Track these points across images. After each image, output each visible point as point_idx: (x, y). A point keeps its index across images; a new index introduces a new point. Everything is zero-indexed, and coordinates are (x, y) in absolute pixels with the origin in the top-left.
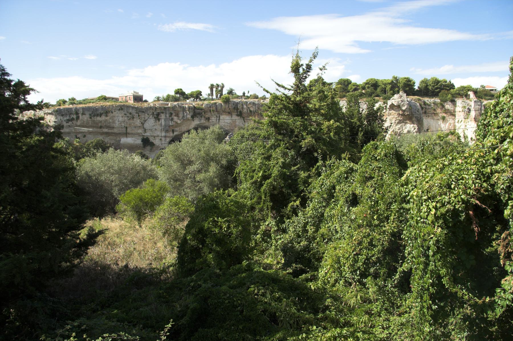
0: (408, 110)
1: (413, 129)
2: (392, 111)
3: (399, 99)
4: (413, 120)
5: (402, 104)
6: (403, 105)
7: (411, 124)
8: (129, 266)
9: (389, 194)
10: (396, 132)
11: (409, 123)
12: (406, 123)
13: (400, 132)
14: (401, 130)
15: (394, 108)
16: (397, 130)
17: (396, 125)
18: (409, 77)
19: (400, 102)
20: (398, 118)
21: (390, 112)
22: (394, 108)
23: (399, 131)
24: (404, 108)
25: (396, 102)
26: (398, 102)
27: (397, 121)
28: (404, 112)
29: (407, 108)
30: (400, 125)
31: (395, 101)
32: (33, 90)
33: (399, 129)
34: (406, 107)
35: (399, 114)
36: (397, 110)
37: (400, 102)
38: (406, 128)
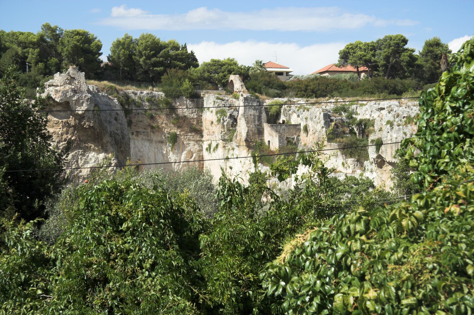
3: (68, 87)
4: (105, 141)
5: (75, 98)
7: (99, 152)
11: (94, 150)
12: (87, 150)
19: (70, 94)
20: (64, 136)
24: (80, 110)
25: (60, 94)
28: (80, 121)
31: (57, 92)
34: (84, 107)
35: (67, 125)
36: (62, 114)
37: (70, 94)
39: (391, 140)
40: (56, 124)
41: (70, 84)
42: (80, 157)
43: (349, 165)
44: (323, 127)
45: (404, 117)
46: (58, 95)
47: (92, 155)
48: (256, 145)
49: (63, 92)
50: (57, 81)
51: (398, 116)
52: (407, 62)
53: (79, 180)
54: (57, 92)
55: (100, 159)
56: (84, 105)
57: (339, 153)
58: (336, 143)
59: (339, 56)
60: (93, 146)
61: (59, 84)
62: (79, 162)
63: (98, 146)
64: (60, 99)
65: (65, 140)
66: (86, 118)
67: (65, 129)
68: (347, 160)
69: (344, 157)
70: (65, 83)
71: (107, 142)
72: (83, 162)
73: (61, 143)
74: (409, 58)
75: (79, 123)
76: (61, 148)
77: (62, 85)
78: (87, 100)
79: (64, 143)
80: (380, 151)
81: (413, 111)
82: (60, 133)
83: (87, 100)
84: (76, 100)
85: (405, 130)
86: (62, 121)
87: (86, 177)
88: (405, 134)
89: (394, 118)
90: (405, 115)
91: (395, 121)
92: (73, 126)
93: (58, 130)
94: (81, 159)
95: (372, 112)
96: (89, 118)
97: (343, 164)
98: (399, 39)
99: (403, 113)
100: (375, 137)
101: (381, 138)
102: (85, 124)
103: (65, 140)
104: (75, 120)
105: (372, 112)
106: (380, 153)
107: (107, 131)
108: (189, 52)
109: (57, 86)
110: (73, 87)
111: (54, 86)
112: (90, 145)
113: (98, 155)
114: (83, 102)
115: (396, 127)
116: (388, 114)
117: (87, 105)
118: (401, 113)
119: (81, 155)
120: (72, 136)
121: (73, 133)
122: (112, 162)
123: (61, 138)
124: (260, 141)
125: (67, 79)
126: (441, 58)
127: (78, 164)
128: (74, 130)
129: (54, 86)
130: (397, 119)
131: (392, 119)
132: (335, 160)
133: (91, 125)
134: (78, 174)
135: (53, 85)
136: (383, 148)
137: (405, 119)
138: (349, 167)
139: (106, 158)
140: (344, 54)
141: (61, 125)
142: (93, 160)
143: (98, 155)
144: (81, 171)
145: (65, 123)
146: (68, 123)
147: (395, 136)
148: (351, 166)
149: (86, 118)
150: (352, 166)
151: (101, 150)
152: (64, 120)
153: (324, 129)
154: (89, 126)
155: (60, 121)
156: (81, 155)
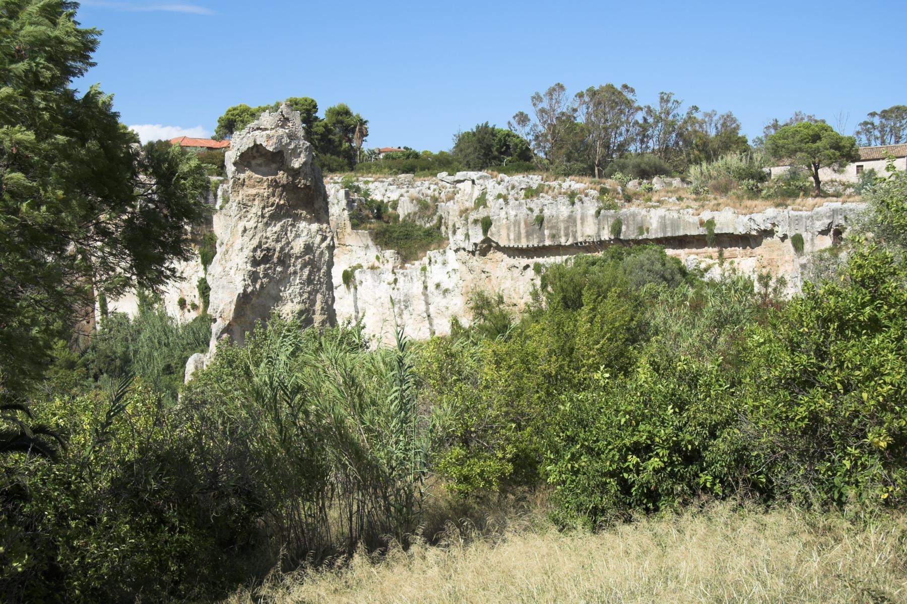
0: (308, 170)
1: (319, 238)
2: (248, 173)
3: (281, 131)
4: (316, 206)
5: (292, 146)
6: (295, 153)
7: (310, 222)
8: (416, 494)
9: (549, 412)
10: (268, 249)
11: (305, 219)
12: (297, 218)
13: (282, 249)
14: (284, 242)
15: (253, 162)
16: (270, 244)
17: (267, 225)
18: (549, 87)
19: (285, 140)
20: (272, 200)
21: (242, 176)
22: (253, 162)
23: (278, 246)
24: (296, 164)
25: (275, 140)
26: (280, 138)
27: (268, 211)
28: (294, 179)
29: (305, 164)
30: (279, 225)
31: (269, 137)
32: (255, 141)
33: (278, 241)
34: (302, 159)
35: (275, 184)
36: (263, 169)
37: (285, 140)
38: (297, 236)
39: (507, 218)
40: (259, 182)
41: (282, 127)
42: (289, 229)
43: (388, 258)
44: (344, 209)
45: (522, 189)
46: (271, 142)
47: (303, 225)
48: (204, 238)
49: (277, 138)
50: (265, 123)
51: (513, 188)
52: (321, 134)
53: (290, 260)
54: (269, 137)
55: (312, 231)
56: (302, 155)
57: (370, 243)
58: (366, 230)
59: (217, 124)
60: (304, 212)
61: (269, 127)
62: (289, 235)
63: (311, 215)
64: (274, 147)
65: (272, 205)
66: (303, 174)
67: (271, 190)
68: (383, 252)
69: (380, 249)
70: (277, 126)
71: (320, 208)
72: (293, 235)
73: (267, 210)
74: (324, 130)
75: (292, 181)
76: (267, 215)
77: (273, 129)
78: (306, 150)
79: (270, 208)
80: (489, 233)
81: (534, 181)
82: (266, 194)
83: (306, 150)
84: (293, 149)
85: (533, 206)
86: (268, 179)
87: (299, 255)
88: (531, 210)
89: (508, 190)
90: (523, 186)
91: (509, 194)
92: (283, 186)
93: (262, 190)
94: (291, 231)
95: (386, 191)
96: (306, 174)
97: (378, 258)
98: (310, 104)
99: (520, 183)
100: (478, 216)
101: (488, 217)
102: (300, 182)
103: (272, 205)
104: (287, 177)
105: (386, 191)
106: (489, 236)
107: (321, 193)
108: (113, 110)
109: (266, 129)
110: (287, 131)
111: (261, 129)
112: (300, 211)
113: (309, 225)
114: (301, 152)
115: (512, 202)
116: (497, 185)
117: (306, 156)
118: (517, 184)
119: (291, 225)
120: (280, 200)
121: (281, 195)
122: (328, 235)
123: (267, 203)
124: (208, 234)
125: (280, 120)
126: (353, 132)
127: (287, 238)
128: (283, 192)
129: (261, 129)
130: (512, 192)
131: (504, 192)
132: (364, 252)
133: (308, 184)
134: (289, 251)
135: (258, 129)
136: (493, 229)
137: (523, 191)
138: (388, 261)
139: (321, 230)
140: (229, 124)
141: (266, 183)
142: (305, 233)
143: (309, 225)
144: (292, 248)
145: (272, 180)
146: (276, 181)
147: (512, 213)
148: (390, 260)
149: (303, 174)
150: (391, 260)
151: (314, 219)
152: (270, 178)
153: (346, 212)
154: (305, 185)
155: (265, 178)
156: (291, 225)
